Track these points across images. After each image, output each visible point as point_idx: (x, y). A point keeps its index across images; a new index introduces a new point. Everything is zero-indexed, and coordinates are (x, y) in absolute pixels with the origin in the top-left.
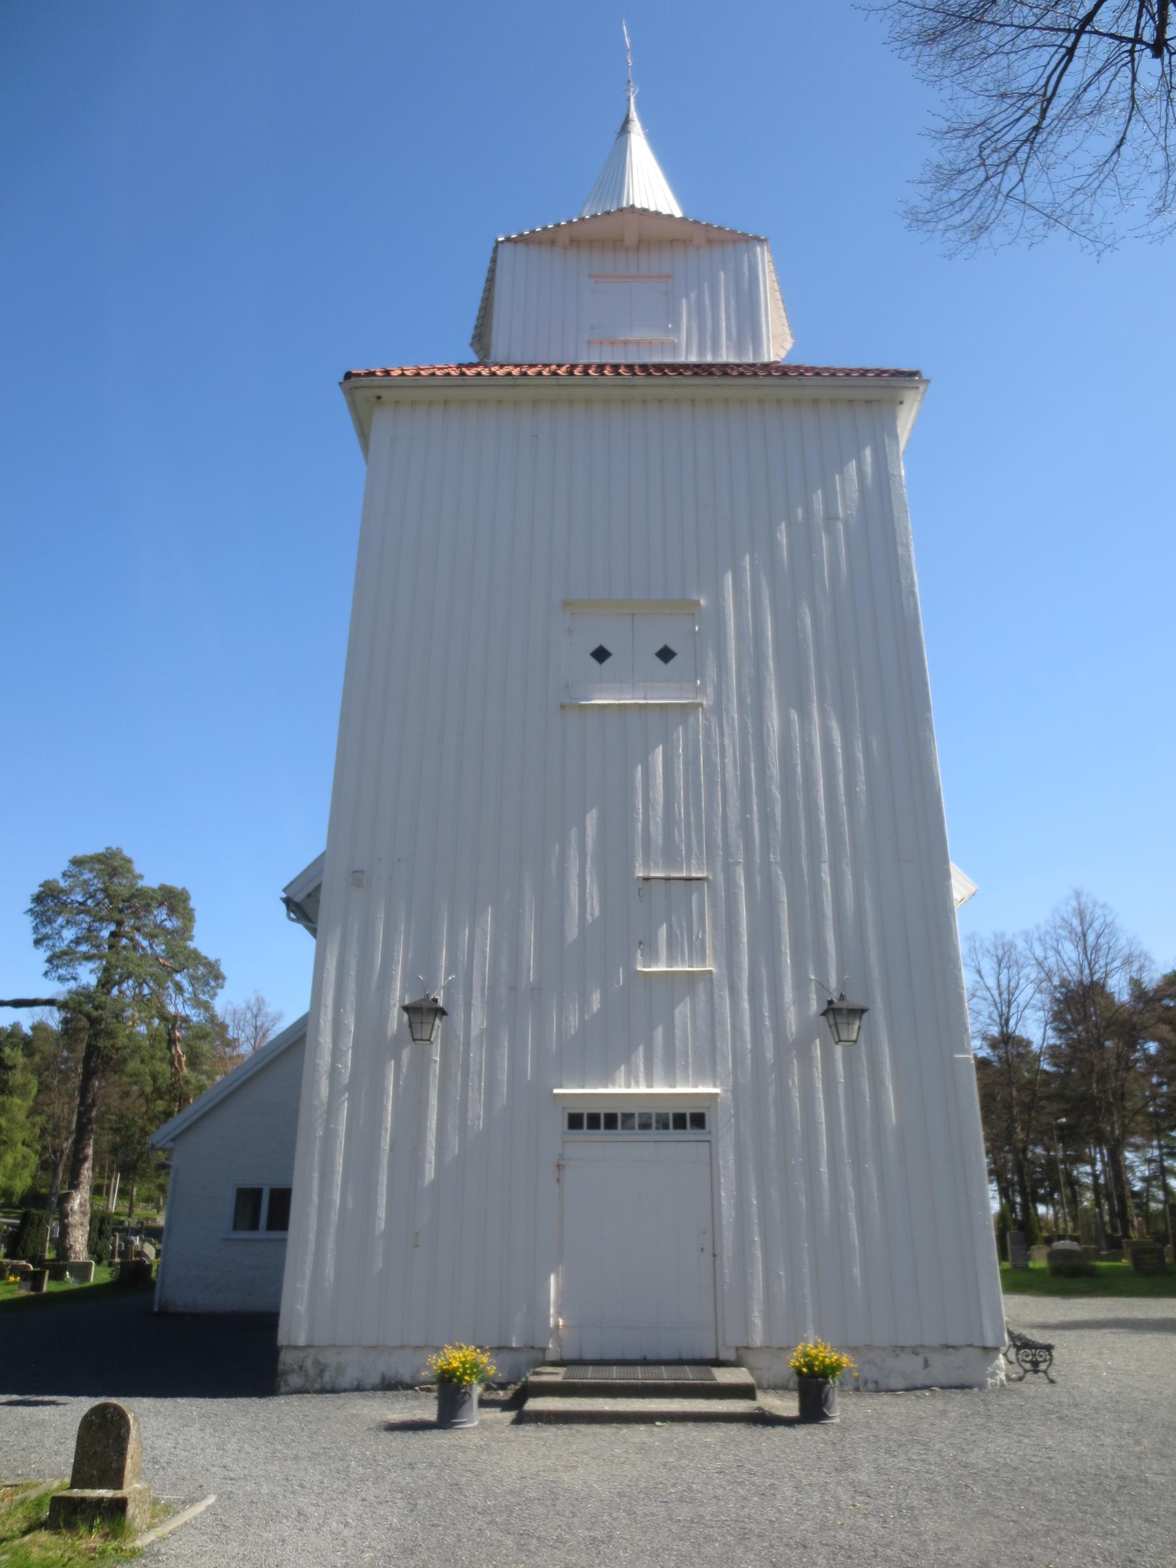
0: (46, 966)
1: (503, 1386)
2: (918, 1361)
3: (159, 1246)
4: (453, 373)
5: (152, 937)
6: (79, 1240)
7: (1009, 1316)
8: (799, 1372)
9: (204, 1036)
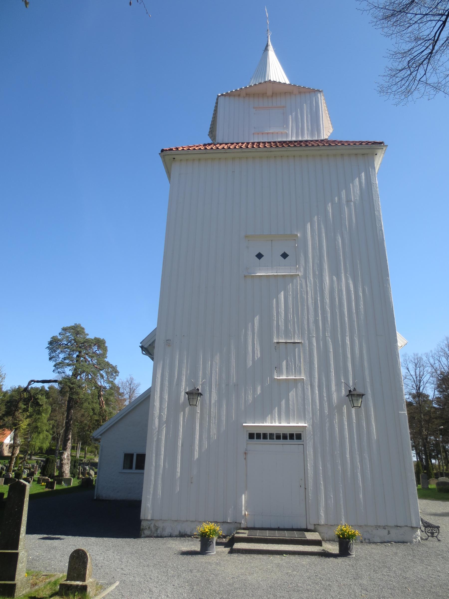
0: (54, 368)
1: (225, 537)
2: (386, 532)
3: (96, 470)
4: (202, 148)
5: (92, 357)
6: (67, 469)
7: (421, 510)
8: (339, 537)
9: (111, 394)
